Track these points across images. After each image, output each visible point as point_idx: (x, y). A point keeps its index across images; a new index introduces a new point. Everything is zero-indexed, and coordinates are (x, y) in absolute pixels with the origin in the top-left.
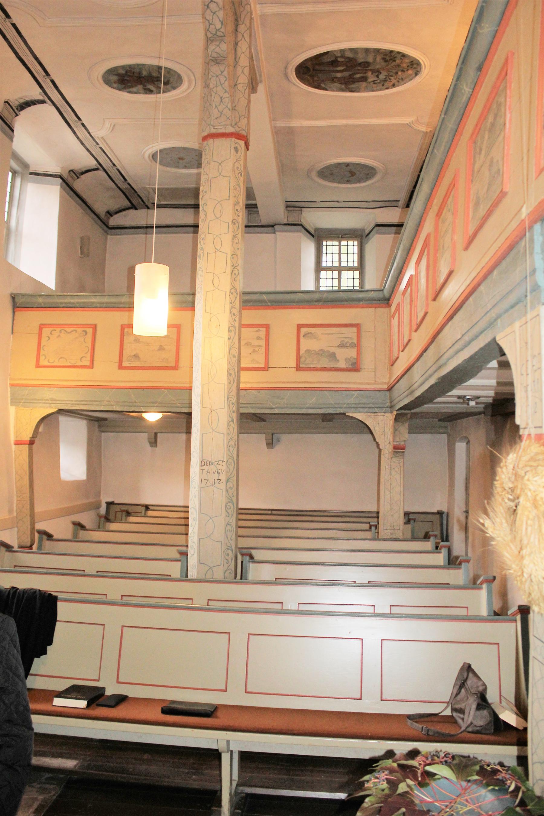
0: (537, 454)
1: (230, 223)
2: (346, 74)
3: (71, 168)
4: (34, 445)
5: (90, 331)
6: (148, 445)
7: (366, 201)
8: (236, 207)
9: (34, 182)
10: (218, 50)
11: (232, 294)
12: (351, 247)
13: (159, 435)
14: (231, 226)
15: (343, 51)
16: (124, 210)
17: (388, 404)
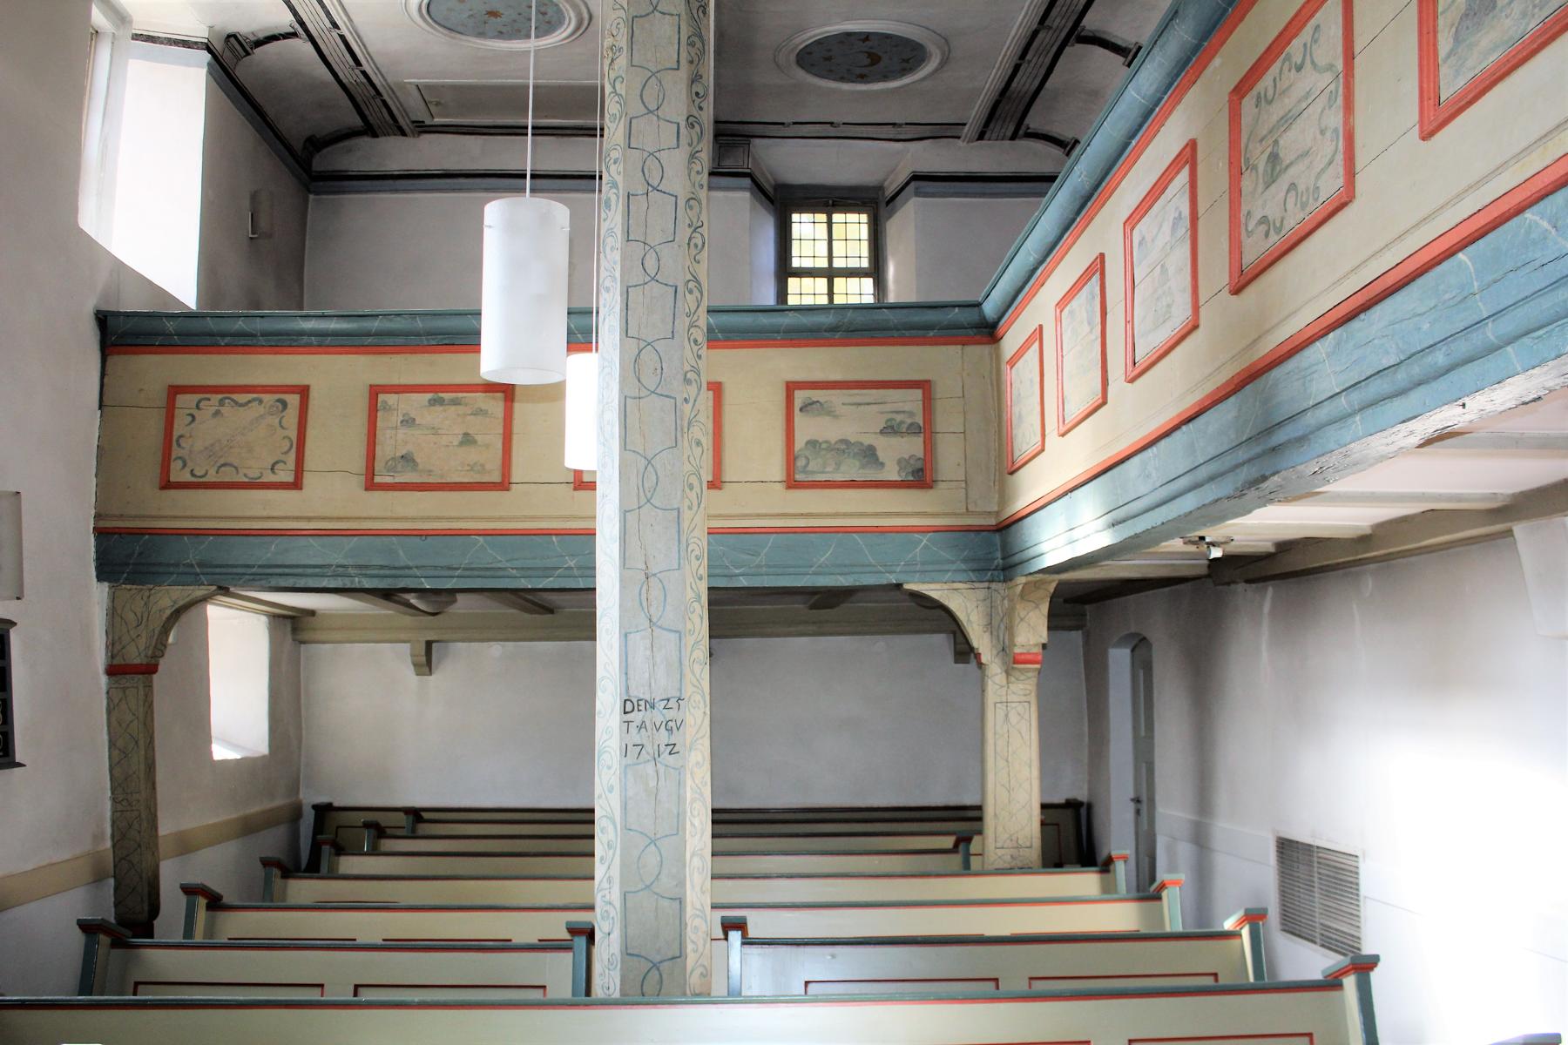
1: (683, 124)
3: (232, 29)
5: (293, 400)
6: (409, 671)
8: (698, 88)
9: (146, 57)
11: (691, 292)
12: (853, 227)
14: (683, 130)
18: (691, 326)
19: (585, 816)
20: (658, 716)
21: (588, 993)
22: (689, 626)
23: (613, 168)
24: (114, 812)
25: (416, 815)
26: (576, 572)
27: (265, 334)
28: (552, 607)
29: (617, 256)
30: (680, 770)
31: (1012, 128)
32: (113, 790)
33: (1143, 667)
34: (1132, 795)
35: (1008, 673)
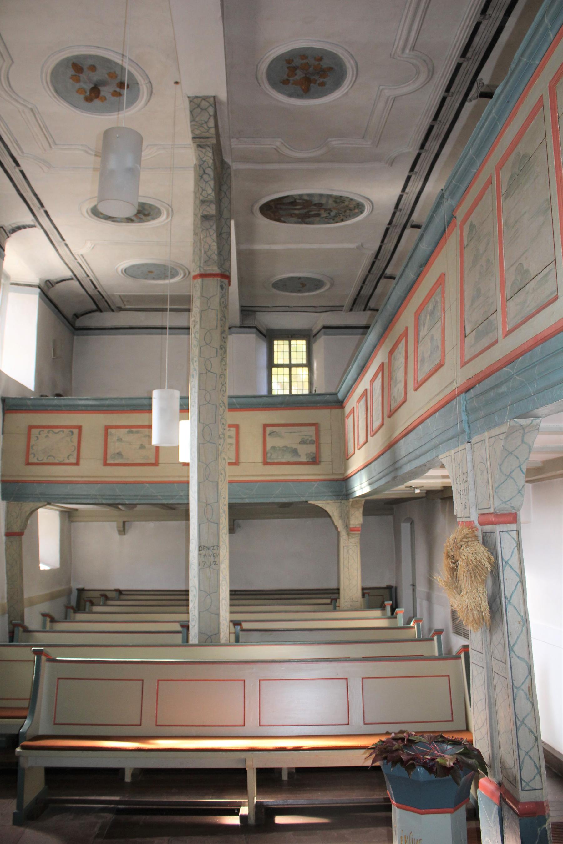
0: (467, 534)
1: (219, 348)
5: (76, 431)
11: (221, 407)
12: (300, 346)
13: (126, 523)
14: (219, 350)
15: (301, 196)
18: (222, 419)
21: (187, 641)
22: (221, 521)
24: (8, 588)
25: (120, 592)
27: (66, 406)
28: (177, 511)
29: (196, 395)
31: (363, 307)
34: (411, 583)
35: (348, 535)
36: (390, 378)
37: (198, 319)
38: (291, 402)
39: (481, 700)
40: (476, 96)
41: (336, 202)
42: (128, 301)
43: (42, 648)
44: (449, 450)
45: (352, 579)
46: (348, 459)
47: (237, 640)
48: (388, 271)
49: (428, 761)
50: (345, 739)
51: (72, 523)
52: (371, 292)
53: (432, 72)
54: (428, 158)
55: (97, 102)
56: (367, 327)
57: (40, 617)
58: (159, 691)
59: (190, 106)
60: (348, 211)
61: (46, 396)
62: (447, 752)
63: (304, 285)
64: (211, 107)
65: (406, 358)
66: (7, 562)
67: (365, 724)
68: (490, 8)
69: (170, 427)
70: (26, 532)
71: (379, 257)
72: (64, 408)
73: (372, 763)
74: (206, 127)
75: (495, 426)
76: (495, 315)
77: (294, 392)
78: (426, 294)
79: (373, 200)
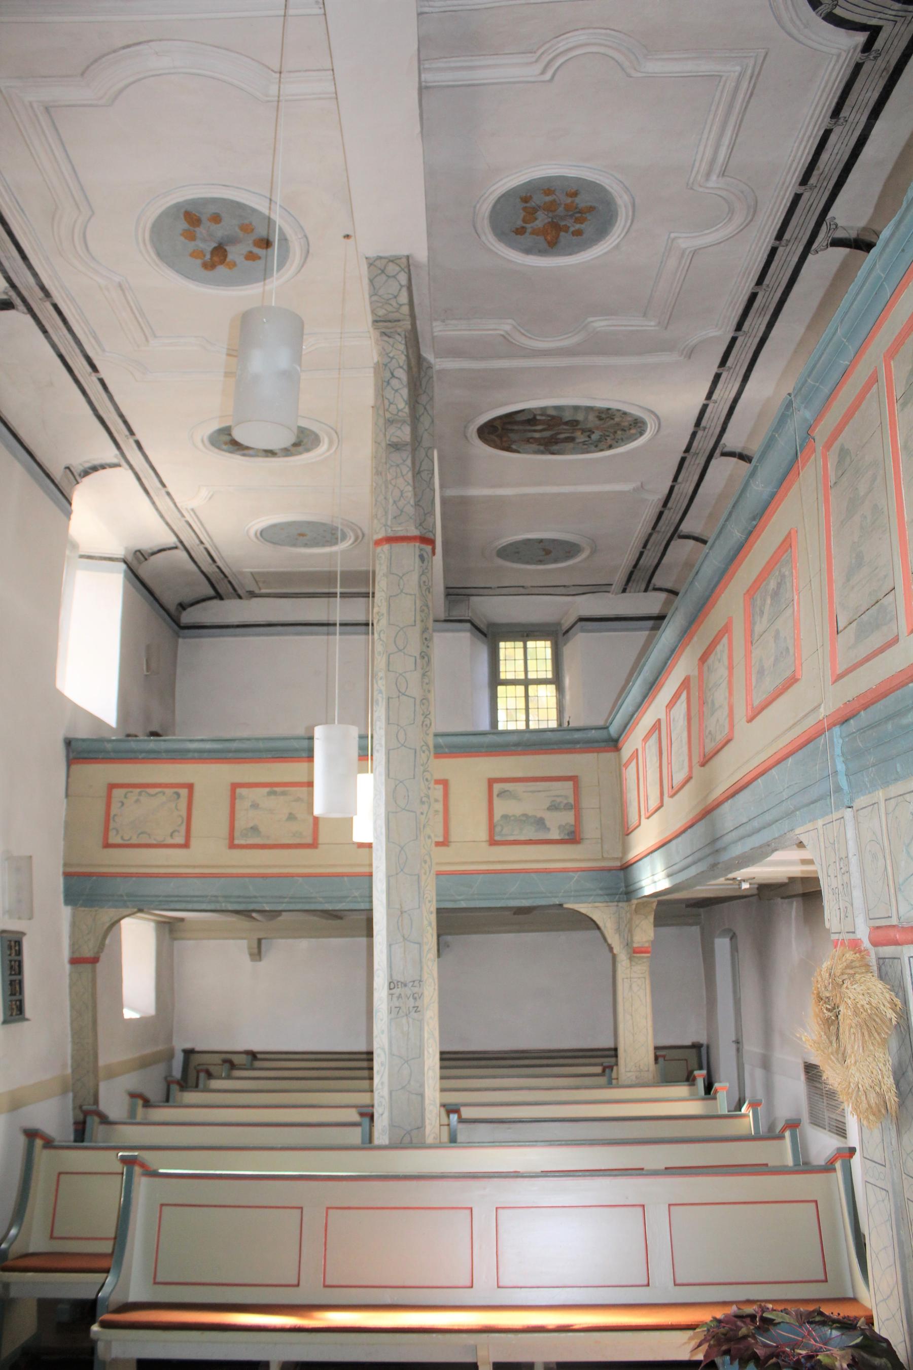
0: (852, 961)
1: (418, 657)
2: (547, 434)
3: (138, 548)
4: (98, 965)
5: (184, 792)
6: (247, 957)
7: (564, 586)
10: (399, 433)
11: (424, 752)
12: (541, 649)
13: (263, 941)
14: (418, 660)
15: (544, 409)
16: (204, 600)
17: (623, 889)
18: (424, 771)
19: (369, 1056)
20: (408, 991)
22: (425, 940)
23: (380, 682)
24: (73, 1050)
25: (253, 1055)
26: (359, 900)
27: (167, 751)
28: (345, 918)
29: (383, 732)
30: (421, 1021)
31: (643, 586)
32: (73, 1037)
33: (734, 949)
34: (734, 1039)
36: (703, 702)
37: (384, 610)
38: (531, 743)
39: (885, 1248)
40: (825, 244)
41: (600, 418)
42: (264, 582)
43: (136, 1154)
44: (813, 820)
45: (638, 1035)
46: (628, 834)
47: (453, 1139)
48: (685, 528)
49: (803, 1360)
50: (644, 1311)
51: (176, 943)
52: (656, 561)
53: (754, 210)
54: (748, 345)
55: (221, 269)
56: (661, 618)
57: (126, 1099)
58: (329, 1228)
59: (369, 272)
60: (619, 432)
61: (136, 736)
62: (832, 1342)
63: (548, 552)
64: (402, 273)
65: (731, 668)
66: (72, 1007)
67: (675, 1285)
68: (845, 107)
69: (344, 787)
70: (103, 957)
71: (669, 505)
72: (164, 755)
73: (692, 1356)
74: (395, 304)
75: (896, 780)
76: (890, 597)
77: (533, 726)
78: (764, 563)
79: (659, 414)
